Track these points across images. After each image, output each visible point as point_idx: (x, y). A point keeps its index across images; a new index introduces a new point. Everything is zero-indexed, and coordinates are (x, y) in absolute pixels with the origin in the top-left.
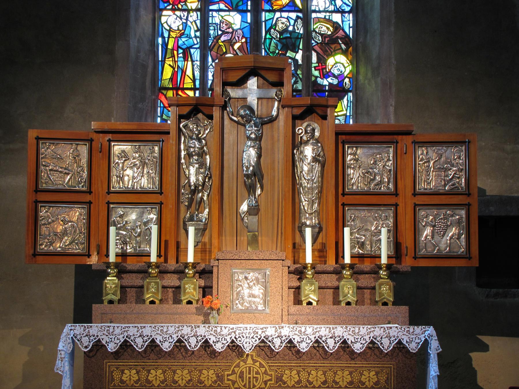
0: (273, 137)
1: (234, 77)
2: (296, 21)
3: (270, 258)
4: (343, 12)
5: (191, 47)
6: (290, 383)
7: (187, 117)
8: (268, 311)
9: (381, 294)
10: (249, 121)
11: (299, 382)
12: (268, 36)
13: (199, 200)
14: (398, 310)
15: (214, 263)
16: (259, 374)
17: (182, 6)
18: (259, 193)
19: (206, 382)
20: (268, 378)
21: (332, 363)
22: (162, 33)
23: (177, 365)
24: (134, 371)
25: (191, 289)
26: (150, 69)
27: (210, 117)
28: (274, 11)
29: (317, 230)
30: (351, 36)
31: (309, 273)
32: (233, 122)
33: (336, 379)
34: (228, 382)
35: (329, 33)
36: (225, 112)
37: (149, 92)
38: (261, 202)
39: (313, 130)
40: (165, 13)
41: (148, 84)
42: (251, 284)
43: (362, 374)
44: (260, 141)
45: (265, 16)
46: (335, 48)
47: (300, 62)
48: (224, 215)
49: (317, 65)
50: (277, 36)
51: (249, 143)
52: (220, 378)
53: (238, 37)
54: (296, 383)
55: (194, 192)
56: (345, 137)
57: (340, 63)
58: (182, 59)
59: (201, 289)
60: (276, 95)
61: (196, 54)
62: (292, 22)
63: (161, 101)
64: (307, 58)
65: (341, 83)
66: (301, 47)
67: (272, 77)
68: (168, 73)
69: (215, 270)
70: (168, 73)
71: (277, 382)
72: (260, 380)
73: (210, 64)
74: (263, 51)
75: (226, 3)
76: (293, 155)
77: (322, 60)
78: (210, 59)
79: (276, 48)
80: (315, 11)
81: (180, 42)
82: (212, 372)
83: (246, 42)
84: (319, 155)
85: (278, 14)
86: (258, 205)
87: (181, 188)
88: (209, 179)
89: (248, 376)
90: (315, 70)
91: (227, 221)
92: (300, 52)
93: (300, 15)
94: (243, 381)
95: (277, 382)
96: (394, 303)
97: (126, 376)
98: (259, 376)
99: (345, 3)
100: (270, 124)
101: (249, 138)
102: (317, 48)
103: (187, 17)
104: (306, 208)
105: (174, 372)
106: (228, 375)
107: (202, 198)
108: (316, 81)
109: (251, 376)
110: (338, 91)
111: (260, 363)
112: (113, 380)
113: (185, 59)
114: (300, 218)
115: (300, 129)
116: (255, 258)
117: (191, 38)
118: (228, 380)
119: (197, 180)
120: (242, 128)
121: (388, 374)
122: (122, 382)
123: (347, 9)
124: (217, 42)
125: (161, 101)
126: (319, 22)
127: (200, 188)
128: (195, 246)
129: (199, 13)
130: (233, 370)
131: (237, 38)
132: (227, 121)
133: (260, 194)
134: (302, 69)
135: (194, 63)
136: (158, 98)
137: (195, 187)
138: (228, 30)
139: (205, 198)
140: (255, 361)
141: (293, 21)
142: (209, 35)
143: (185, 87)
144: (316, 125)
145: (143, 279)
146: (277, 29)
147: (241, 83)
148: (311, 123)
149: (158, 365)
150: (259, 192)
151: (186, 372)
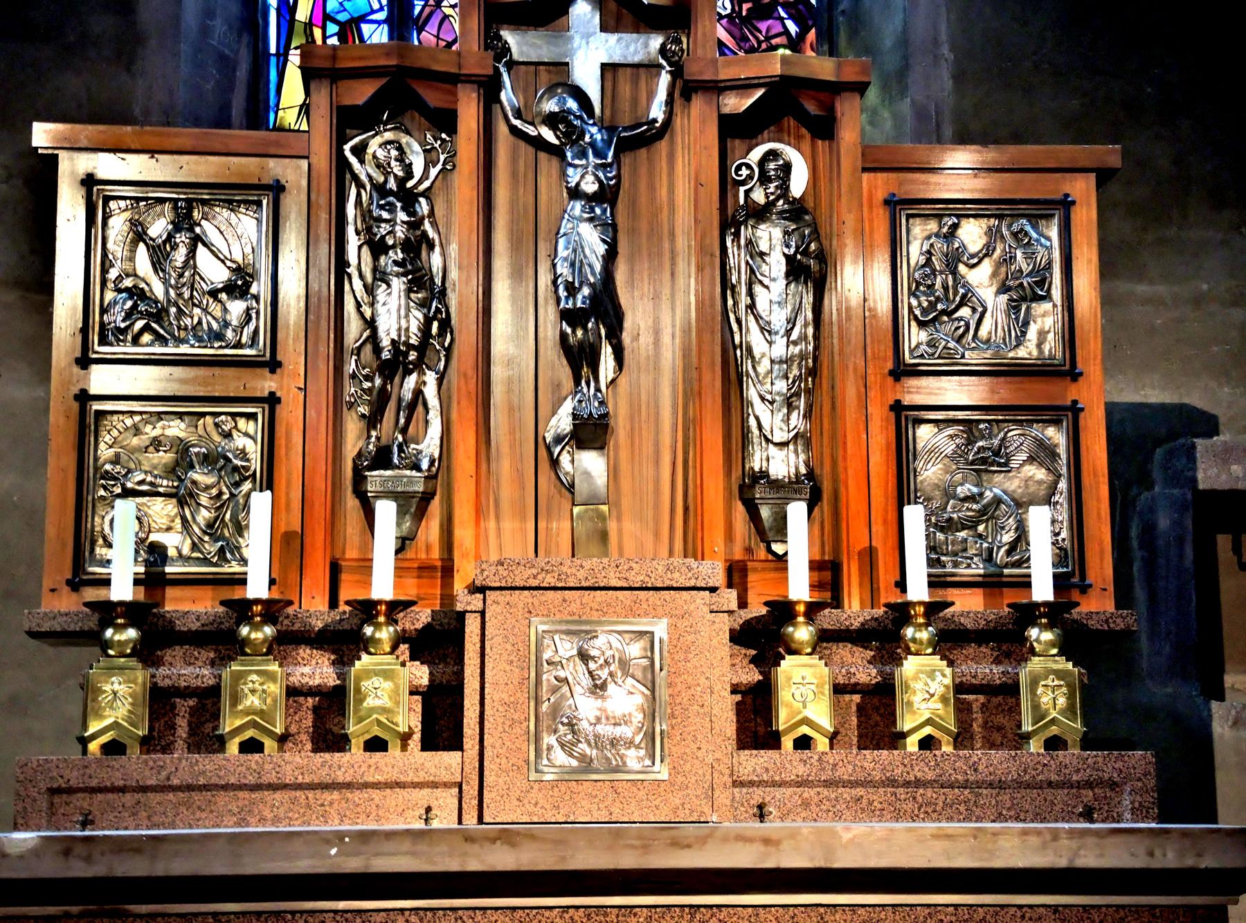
3: (667, 583)
5: (363, 19)
9: (1039, 714)
14: (1119, 765)
15: (465, 601)
18: (611, 376)
25: (387, 686)
26: (242, 73)
38: (616, 404)
39: (787, 168)
42: (604, 674)
46: (768, 30)
48: (493, 443)
51: (577, 207)
59: (419, 698)
69: (472, 626)
86: (606, 415)
87: (346, 356)
91: (504, 467)
96: (1087, 743)
107: (418, 393)
116: (614, 583)
120: (547, 164)
127: (413, 356)
128: (397, 552)
133: (613, 381)
145: (222, 660)
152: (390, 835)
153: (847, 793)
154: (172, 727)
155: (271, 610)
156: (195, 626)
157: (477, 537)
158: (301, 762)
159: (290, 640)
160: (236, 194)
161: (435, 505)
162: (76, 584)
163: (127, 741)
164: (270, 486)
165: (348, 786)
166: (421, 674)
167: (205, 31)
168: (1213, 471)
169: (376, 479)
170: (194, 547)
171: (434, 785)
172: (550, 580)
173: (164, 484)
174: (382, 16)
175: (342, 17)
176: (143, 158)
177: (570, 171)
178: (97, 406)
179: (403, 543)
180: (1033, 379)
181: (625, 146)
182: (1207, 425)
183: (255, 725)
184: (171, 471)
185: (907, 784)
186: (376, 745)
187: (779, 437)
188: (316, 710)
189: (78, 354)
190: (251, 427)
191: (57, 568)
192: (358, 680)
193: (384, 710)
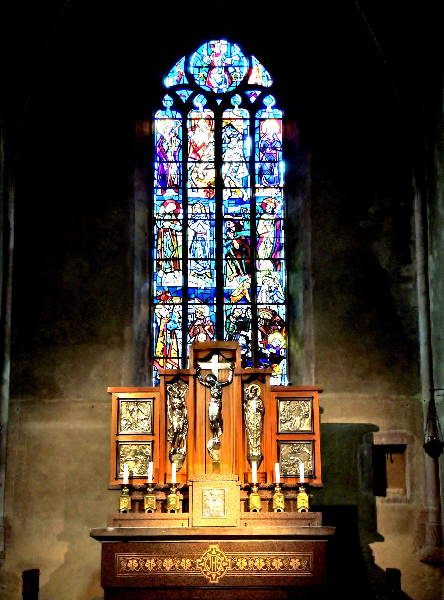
0: (229, 395)
1: (202, 355)
2: (247, 310)
4: (278, 304)
6: (242, 568)
7: (171, 382)
8: (226, 516)
10: (213, 385)
11: (247, 567)
12: (228, 321)
13: (180, 439)
15: (189, 484)
16: (220, 562)
17: (169, 302)
19: (184, 568)
20: (227, 564)
21: (270, 553)
22: (156, 320)
23: (164, 556)
24: (135, 561)
25: (175, 499)
26: (148, 345)
27: (187, 382)
28: (232, 304)
29: (260, 459)
30: (284, 321)
31: (255, 489)
32: (202, 386)
33: (273, 565)
34: (199, 568)
35: (270, 318)
36: (197, 379)
37: (147, 361)
39: (256, 390)
40: (158, 306)
41: (146, 352)
43: (290, 561)
44: (221, 398)
45: (225, 307)
47: (250, 338)
49: (262, 340)
50: (234, 321)
51: (213, 400)
52: (194, 565)
53: (208, 322)
54: (245, 567)
55: (176, 434)
56: (280, 394)
57: (277, 339)
58: (170, 337)
60: (231, 367)
61: (179, 334)
62: (244, 311)
63: (155, 367)
64: (255, 336)
65: (278, 352)
66: (250, 328)
67: (228, 356)
68: (160, 347)
69: (190, 488)
70: (160, 347)
71: (232, 567)
72: (221, 566)
73: (188, 340)
74: (225, 331)
75: (199, 299)
76: (243, 407)
77: (265, 337)
78: (188, 337)
79: (234, 329)
80: (260, 304)
81: (168, 326)
82: (188, 560)
83: (213, 325)
84: (260, 407)
85: (234, 306)
88: (187, 425)
89: (213, 563)
90: (261, 343)
91: (199, 453)
92: (250, 332)
93: (250, 306)
94: (209, 567)
95: (232, 567)
97: (148, 564)
98: (220, 563)
99: (280, 298)
100: (227, 387)
101: (213, 396)
102: (261, 328)
103: (173, 309)
104: (252, 444)
105: (163, 561)
106: (199, 563)
107: (182, 438)
108: (261, 351)
109: (215, 563)
110: (276, 359)
111: (221, 554)
112: (121, 567)
113: (172, 337)
114: (248, 450)
115: (248, 388)
117: (176, 323)
118: (199, 566)
119: (179, 425)
120: (208, 389)
121: (307, 561)
122: (128, 568)
123: (282, 302)
124: (193, 325)
125: (155, 367)
126: (263, 311)
127: (181, 431)
129: (181, 306)
130: (203, 559)
131: (207, 322)
132: (198, 385)
134: (252, 343)
135: (178, 340)
136: (153, 363)
137: (177, 430)
138: (200, 317)
139: (184, 438)
140: (217, 553)
141: (245, 311)
142: (188, 321)
143: (172, 356)
144: (257, 386)
146: (234, 316)
147: (207, 359)
148: (255, 385)
149: (152, 556)
150: (220, 433)
151: (153, 560)
152: (174, 529)
153: (262, 521)
154: (135, 507)
155: (153, 485)
156: (139, 487)
157: (193, 469)
158: (159, 515)
159: (157, 490)
160: (145, 400)
161: (185, 461)
162: (117, 479)
163: (127, 510)
164: (153, 461)
165: (167, 519)
166: (182, 497)
167: (139, 337)
168: (378, 440)
169: (174, 456)
170: (138, 471)
171: (183, 519)
172: (205, 480)
173: (133, 459)
174: (180, 328)
175: (171, 329)
176: (128, 393)
177: (212, 392)
178: (120, 443)
179: (179, 470)
180: (428, 367)
181: (223, 386)
182: (377, 429)
183: (151, 508)
184: (133, 456)
185: (274, 519)
186: (173, 511)
187: (255, 446)
188: (162, 504)
189: (116, 433)
190: (149, 447)
191: (113, 476)
192: (169, 499)
193: (174, 505)
